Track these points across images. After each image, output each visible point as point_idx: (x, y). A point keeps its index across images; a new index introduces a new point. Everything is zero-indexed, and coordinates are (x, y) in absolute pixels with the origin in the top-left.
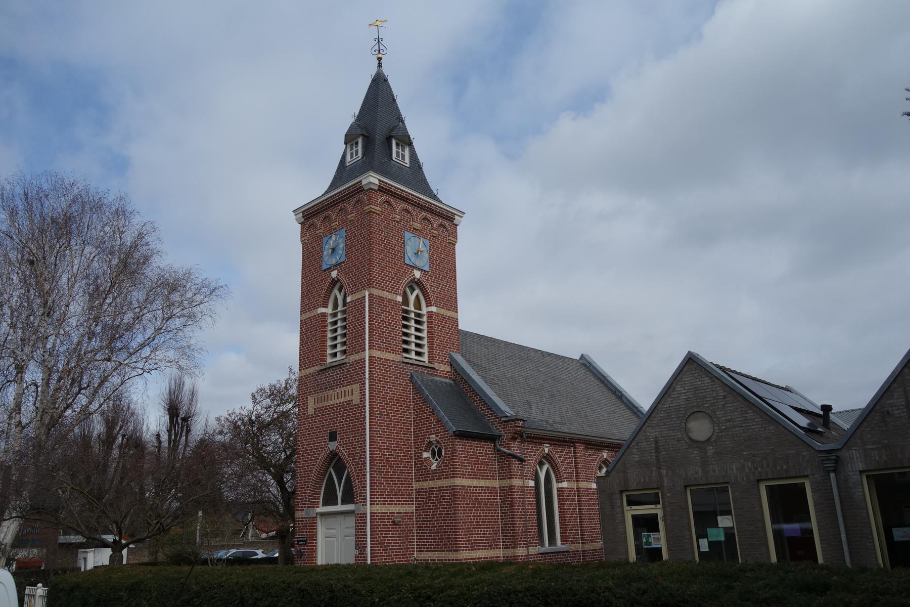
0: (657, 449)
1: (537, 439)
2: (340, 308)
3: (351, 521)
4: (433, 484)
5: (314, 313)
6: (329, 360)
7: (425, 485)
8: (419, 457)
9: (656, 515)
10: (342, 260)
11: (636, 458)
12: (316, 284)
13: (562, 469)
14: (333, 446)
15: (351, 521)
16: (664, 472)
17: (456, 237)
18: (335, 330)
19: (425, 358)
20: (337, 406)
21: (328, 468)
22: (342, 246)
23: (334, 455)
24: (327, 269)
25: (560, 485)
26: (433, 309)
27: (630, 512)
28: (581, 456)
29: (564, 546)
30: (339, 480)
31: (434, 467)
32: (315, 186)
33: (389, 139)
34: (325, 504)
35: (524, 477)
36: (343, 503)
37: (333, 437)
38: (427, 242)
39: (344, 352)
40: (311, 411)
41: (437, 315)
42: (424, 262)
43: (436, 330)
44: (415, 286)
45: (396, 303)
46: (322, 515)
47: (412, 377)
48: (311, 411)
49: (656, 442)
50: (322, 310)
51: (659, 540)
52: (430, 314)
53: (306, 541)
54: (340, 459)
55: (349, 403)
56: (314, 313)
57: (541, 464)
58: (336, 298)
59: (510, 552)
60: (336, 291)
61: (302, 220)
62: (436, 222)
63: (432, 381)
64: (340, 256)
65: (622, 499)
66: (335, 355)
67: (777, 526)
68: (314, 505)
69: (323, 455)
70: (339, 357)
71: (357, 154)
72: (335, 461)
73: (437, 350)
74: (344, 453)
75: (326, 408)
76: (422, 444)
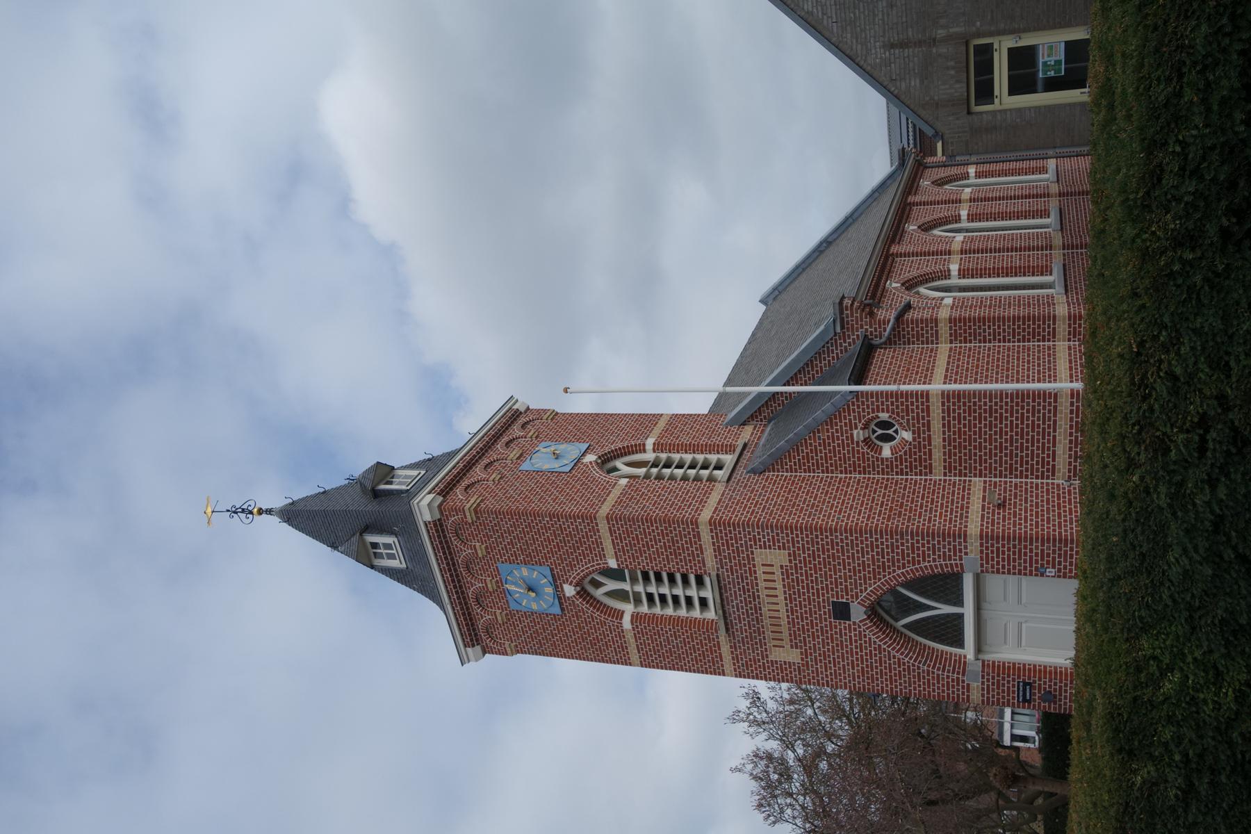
0: (903, 45)
1: (876, 293)
2: (626, 586)
4: (937, 440)
5: (630, 637)
6: (711, 614)
7: (937, 455)
8: (889, 466)
9: (1010, 50)
10: (548, 573)
11: (916, 82)
12: (579, 633)
14: (858, 612)
15: (996, 584)
16: (941, 33)
17: (545, 411)
18: (663, 598)
19: (729, 459)
21: (895, 630)
22: (525, 572)
23: (874, 612)
24: (561, 604)
25: (954, 272)
26: (650, 443)
27: (1005, 99)
28: (911, 249)
29: (1052, 214)
30: (921, 602)
31: (907, 435)
32: (432, 623)
33: (376, 494)
34: (959, 643)
36: (959, 602)
37: (842, 611)
38: (544, 444)
39: (700, 582)
40: (794, 656)
41: (661, 436)
42: (572, 451)
43: (685, 440)
45: (629, 486)
46: (979, 650)
47: (753, 471)
48: (794, 656)
49: (892, 46)
50: (626, 622)
51: (1050, 46)
52: (658, 447)
53: (1025, 684)
55: (786, 573)
56: (630, 637)
58: (611, 594)
59: (1062, 328)
60: (599, 593)
61: (478, 648)
62: (516, 431)
64: (539, 575)
65: (981, 113)
66: (703, 602)
67: (1040, 85)
68: (961, 664)
69: (873, 635)
70: (707, 593)
71: (388, 546)
73: (716, 440)
74: (872, 589)
75: (792, 623)
76: (866, 463)
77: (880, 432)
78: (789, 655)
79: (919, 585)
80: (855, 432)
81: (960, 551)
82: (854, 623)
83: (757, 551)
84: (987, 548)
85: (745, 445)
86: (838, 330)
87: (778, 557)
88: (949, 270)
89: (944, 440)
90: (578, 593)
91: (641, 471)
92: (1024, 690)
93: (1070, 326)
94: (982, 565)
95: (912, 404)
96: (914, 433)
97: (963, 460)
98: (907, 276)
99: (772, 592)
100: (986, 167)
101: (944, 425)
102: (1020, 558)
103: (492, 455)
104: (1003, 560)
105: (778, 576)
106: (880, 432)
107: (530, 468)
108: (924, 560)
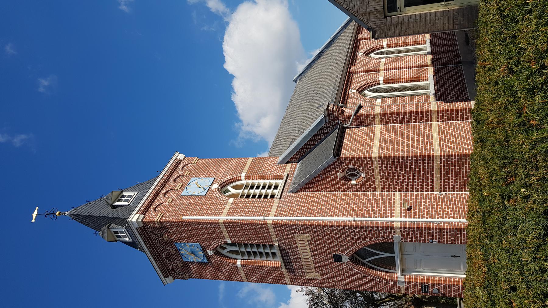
1: (343, 98)
3: (409, 247)
13: (369, 81)
14: (345, 259)
19: (281, 182)
20: (313, 254)
23: (353, 259)
25: (381, 82)
26: (243, 175)
28: (360, 69)
35: (374, 105)
37: (338, 258)
38: (192, 179)
40: (318, 276)
43: (260, 173)
44: (224, 189)
45: (234, 203)
48: (318, 276)
52: (247, 178)
53: (425, 286)
54: (356, 253)
55: (310, 243)
57: (364, 95)
58: (230, 252)
60: (224, 252)
62: (179, 171)
63: (297, 177)
69: (354, 268)
72: (358, 257)
73: (274, 173)
74: (352, 249)
77: (350, 173)
78: (314, 275)
79: (374, 246)
80: (338, 174)
81: (391, 233)
82: (344, 263)
83: (296, 235)
84: (404, 232)
85: (288, 175)
86: (327, 121)
87: (306, 237)
88: (379, 81)
89: (381, 176)
90: (214, 253)
91: (240, 192)
92: (425, 289)
93: (438, 115)
94: (402, 239)
95: (364, 161)
96: (366, 174)
97: (389, 185)
98: (359, 85)
99: (305, 251)
100: (393, 39)
101: (380, 170)
102: (420, 236)
103: (167, 187)
104: (412, 237)
105: (307, 245)
106: (350, 173)
107: (187, 194)
108: (375, 238)
